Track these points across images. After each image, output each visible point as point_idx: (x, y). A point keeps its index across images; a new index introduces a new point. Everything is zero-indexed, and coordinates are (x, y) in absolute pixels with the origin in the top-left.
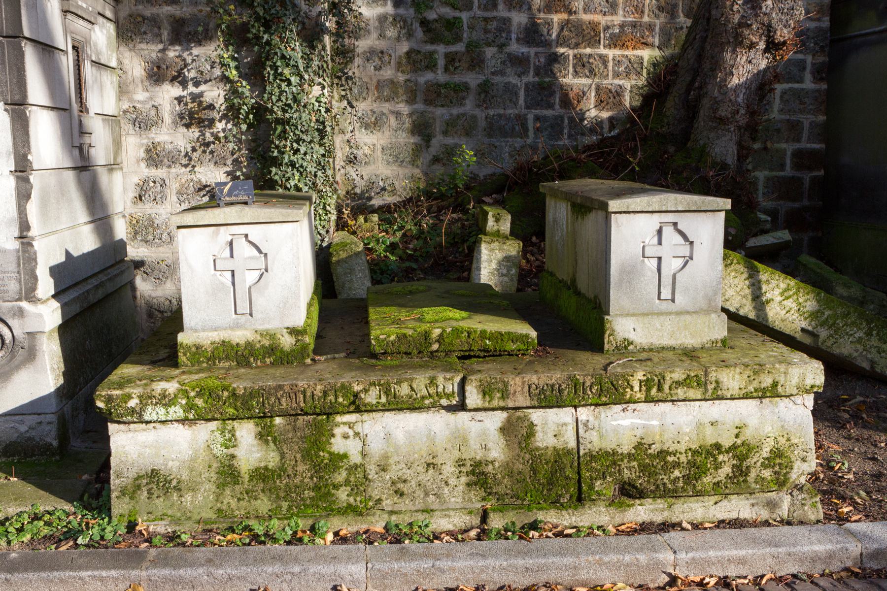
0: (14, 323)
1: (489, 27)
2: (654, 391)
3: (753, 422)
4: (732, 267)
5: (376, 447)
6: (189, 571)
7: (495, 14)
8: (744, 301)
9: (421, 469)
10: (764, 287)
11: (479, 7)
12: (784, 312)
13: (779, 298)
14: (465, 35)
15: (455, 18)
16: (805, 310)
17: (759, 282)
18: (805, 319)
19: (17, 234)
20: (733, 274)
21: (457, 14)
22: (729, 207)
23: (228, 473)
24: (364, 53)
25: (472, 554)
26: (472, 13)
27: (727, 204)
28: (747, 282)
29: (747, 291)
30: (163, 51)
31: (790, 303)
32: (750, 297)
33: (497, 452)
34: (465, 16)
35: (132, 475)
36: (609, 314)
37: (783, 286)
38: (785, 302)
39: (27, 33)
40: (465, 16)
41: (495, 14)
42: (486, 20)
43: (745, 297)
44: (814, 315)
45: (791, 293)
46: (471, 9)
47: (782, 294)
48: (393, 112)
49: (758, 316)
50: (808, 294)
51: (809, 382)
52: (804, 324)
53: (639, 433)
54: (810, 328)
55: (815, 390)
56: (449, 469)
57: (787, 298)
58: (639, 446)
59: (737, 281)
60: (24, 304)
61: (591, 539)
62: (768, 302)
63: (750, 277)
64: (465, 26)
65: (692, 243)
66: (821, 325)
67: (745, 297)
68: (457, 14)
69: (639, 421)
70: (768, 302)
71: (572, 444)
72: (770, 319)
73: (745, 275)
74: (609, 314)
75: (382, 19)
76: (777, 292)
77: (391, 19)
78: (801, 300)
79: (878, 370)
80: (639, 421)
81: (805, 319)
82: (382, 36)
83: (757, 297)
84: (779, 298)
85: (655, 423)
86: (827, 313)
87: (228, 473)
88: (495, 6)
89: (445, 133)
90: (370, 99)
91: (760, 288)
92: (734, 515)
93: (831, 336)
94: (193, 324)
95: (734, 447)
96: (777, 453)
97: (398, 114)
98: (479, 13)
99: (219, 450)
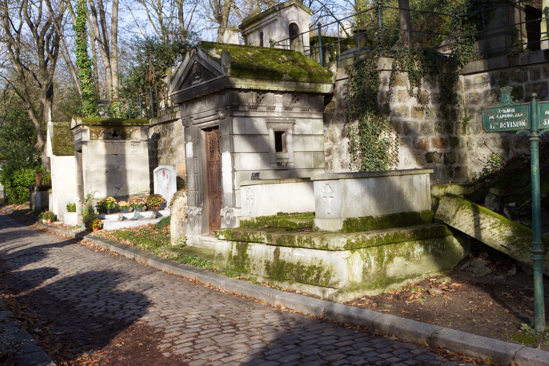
1: (536, 88)
3: (325, 259)
4: (465, 210)
7: (539, 81)
8: (470, 227)
10: (481, 221)
11: (531, 79)
12: (491, 235)
13: (489, 228)
14: (524, 95)
15: (519, 87)
16: (503, 235)
17: (479, 218)
18: (503, 240)
20: (465, 213)
21: (520, 84)
24: (479, 111)
26: (527, 83)
28: (472, 218)
29: (473, 223)
30: (344, 126)
31: (495, 231)
32: (473, 226)
33: (272, 259)
34: (523, 85)
37: (493, 221)
38: (492, 230)
40: (523, 85)
41: (539, 81)
42: (534, 85)
43: (470, 225)
44: (508, 239)
45: (497, 225)
46: (527, 80)
47: (491, 226)
48: (491, 138)
49: (476, 236)
50: (507, 227)
52: (502, 243)
54: (505, 245)
56: (263, 263)
57: (494, 228)
58: (299, 263)
59: (466, 217)
60: (233, 209)
61: (275, 290)
62: (482, 229)
63: (474, 215)
64: (524, 90)
66: (512, 245)
67: (470, 225)
68: (520, 84)
70: (482, 229)
72: (483, 238)
73: (472, 214)
75: (486, 93)
76: (488, 224)
77: (490, 92)
78: (502, 230)
81: (503, 240)
82: (486, 101)
83: (477, 227)
84: (489, 228)
85: (303, 255)
86: (517, 238)
88: (539, 77)
89: (516, 147)
90: (481, 133)
91: (479, 222)
92: (313, 293)
93: (519, 251)
95: (319, 268)
96: (328, 273)
97: (494, 139)
98: (531, 82)
99: (230, 250)
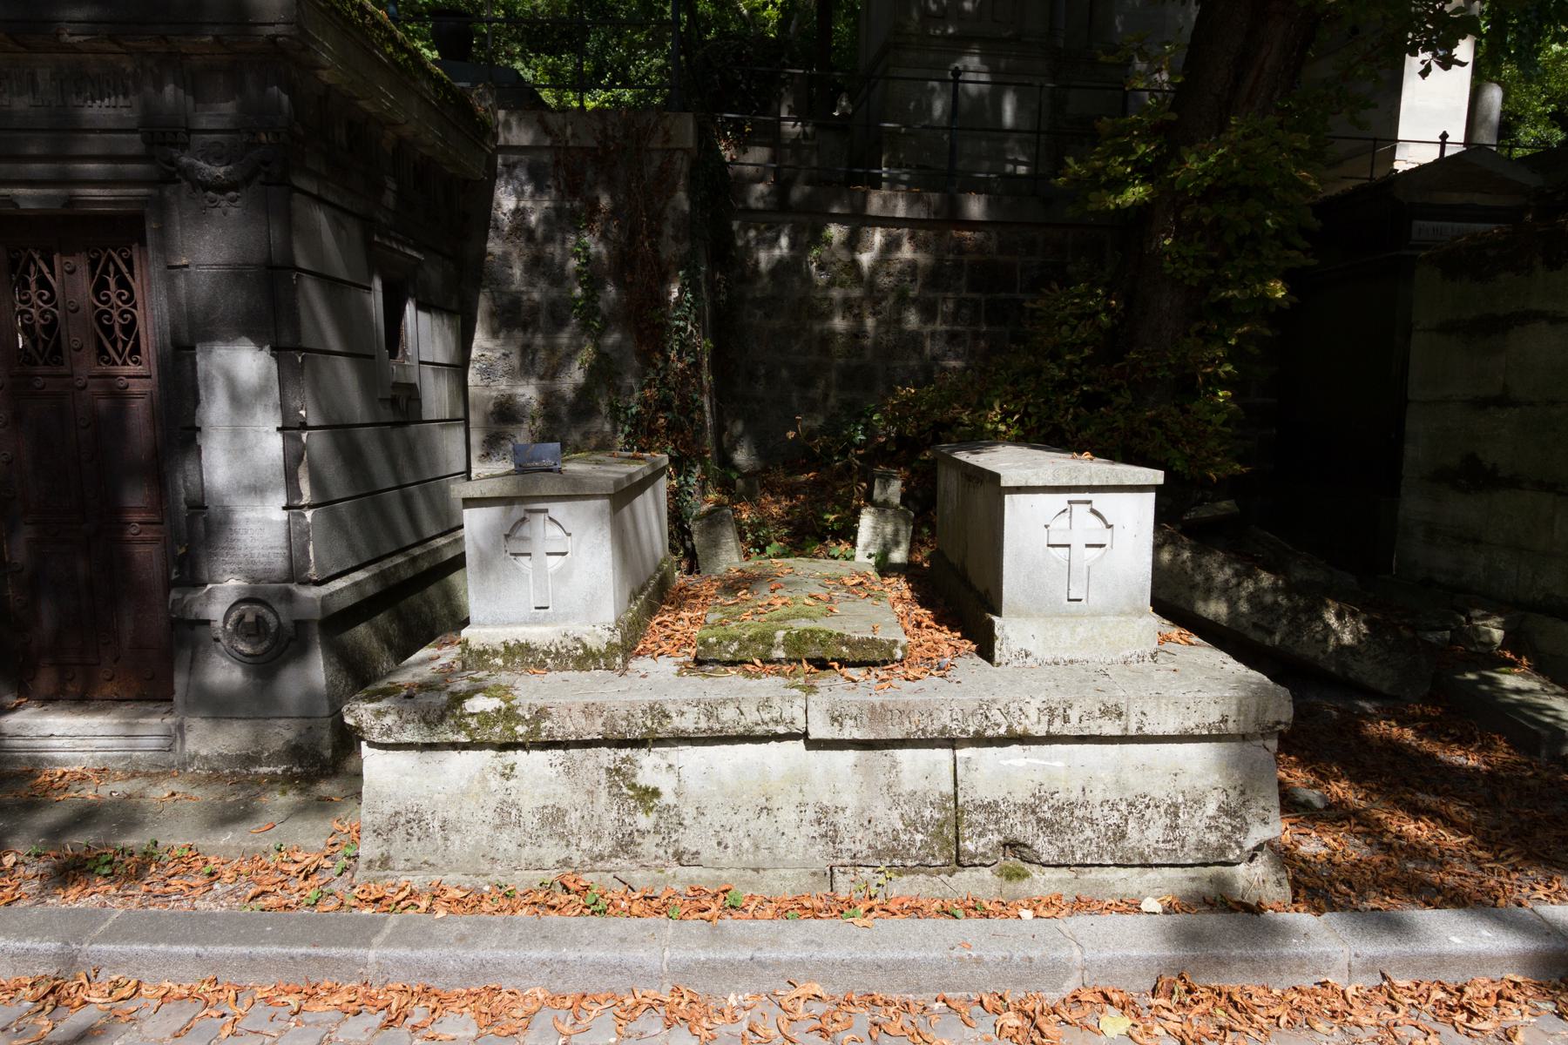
0: (281, 608)
2: (1058, 723)
5: (693, 784)
6: (429, 951)
9: (750, 814)
19: (284, 504)
22: (1161, 481)
23: (506, 814)
25: (805, 942)
27: (1157, 477)
35: (388, 809)
36: (999, 614)
39: (302, 263)
51: (1270, 718)
53: (1038, 777)
55: (1280, 727)
56: (788, 816)
60: (293, 587)
65: (1110, 527)
69: (1037, 761)
71: (948, 788)
74: (999, 614)
79: (1351, 675)
80: (1037, 761)
87: (506, 814)
94: (481, 618)
